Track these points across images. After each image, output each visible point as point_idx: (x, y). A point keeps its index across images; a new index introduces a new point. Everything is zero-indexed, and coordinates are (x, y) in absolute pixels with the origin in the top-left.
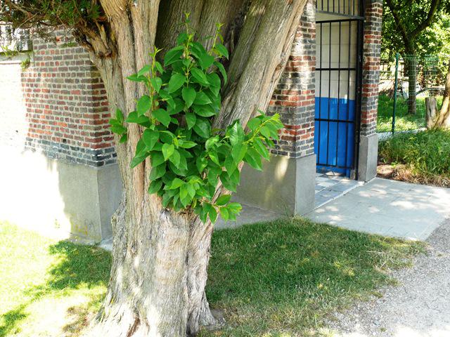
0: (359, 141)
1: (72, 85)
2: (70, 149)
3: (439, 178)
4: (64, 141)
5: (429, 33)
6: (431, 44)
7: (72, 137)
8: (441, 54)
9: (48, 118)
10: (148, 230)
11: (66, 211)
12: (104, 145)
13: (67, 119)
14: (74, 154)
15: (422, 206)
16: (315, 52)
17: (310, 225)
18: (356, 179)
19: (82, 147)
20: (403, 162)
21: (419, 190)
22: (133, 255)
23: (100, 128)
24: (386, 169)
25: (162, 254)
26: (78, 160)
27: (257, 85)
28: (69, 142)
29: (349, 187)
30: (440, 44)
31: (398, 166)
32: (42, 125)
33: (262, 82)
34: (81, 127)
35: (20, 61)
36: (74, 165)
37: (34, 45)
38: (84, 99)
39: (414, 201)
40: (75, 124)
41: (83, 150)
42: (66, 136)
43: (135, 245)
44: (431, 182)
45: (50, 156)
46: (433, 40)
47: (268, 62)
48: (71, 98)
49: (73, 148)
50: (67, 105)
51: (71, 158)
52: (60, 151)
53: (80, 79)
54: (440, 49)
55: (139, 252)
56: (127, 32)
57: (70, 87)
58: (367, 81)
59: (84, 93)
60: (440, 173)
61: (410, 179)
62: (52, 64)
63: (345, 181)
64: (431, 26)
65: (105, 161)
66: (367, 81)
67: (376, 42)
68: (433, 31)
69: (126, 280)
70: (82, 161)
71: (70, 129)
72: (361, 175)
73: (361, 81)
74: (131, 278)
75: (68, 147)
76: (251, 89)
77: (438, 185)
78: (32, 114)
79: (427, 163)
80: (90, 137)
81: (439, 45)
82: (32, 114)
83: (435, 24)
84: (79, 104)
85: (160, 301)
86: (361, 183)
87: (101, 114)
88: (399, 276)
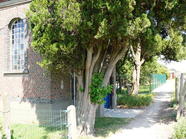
0: (112, 98)
1: (44, 82)
2: (41, 100)
3: (134, 107)
4: (39, 98)
5: (124, 67)
6: (124, 71)
7: (42, 96)
8: (127, 74)
9: (33, 91)
10: (87, 108)
11: (38, 118)
12: (53, 98)
13: (40, 92)
14: (42, 101)
15: (131, 113)
16: (10, 63)
17: (105, 117)
18: (112, 109)
19: (46, 99)
20: (123, 104)
21: (129, 110)
22: (83, 114)
23: (52, 94)
24: (119, 107)
25: (91, 112)
26: (44, 103)
27: (106, 80)
28: (41, 98)
29: (110, 111)
30: (127, 71)
31: (122, 106)
32: (30, 94)
33: (107, 80)
34: (46, 93)
35: (22, 76)
36: (43, 104)
37: (29, 71)
38: (48, 86)
39: (128, 112)
40: (44, 93)
41: (46, 100)
42: (40, 96)
43: (83, 112)
44: (132, 108)
45: (33, 103)
46: (125, 69)
47: (108, 76)
48: (43, 86)
49: (42, 99)
50: (41, 88)
51: (41, 102)
52: (37, 101)
53: (47, 81)
54: (127, 72)
55: (84, 114)
56: (89, 71)
57: (43, 83)
58: (113, 82)
59: (48, 84)
60: (134, 106)
61: (126, 108)
62: (36, 77)
63: (109, 109)
64: (124, 65)
65: (53, 102)
66: (113, 82)
67: (115, 71)
68: (124, 66)
69: (80, 120)
70: (46, 103)
71: (42, 94)
72: (113, 108)
73: (111, 82)
74: (82, 120)
75: (40, 99)
76: (105, 81)
77: (134, 109)
78: (26, 91)
79: (130, 103)
80: (49, 96)
81: (127, 71)
82: (26, 91)
83: (125, 64)
84: (46, 87)
85: (89, 123)
86: (113, 110)
87: (52, 90)
88: (131, 122)
